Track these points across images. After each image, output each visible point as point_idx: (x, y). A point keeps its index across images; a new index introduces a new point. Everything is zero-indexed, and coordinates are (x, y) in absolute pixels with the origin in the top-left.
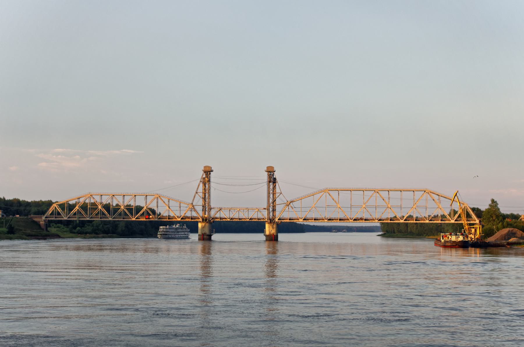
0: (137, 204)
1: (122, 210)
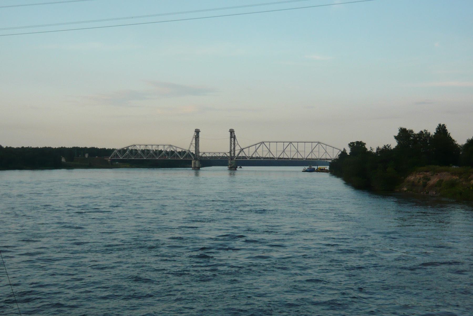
0: (160, 149)
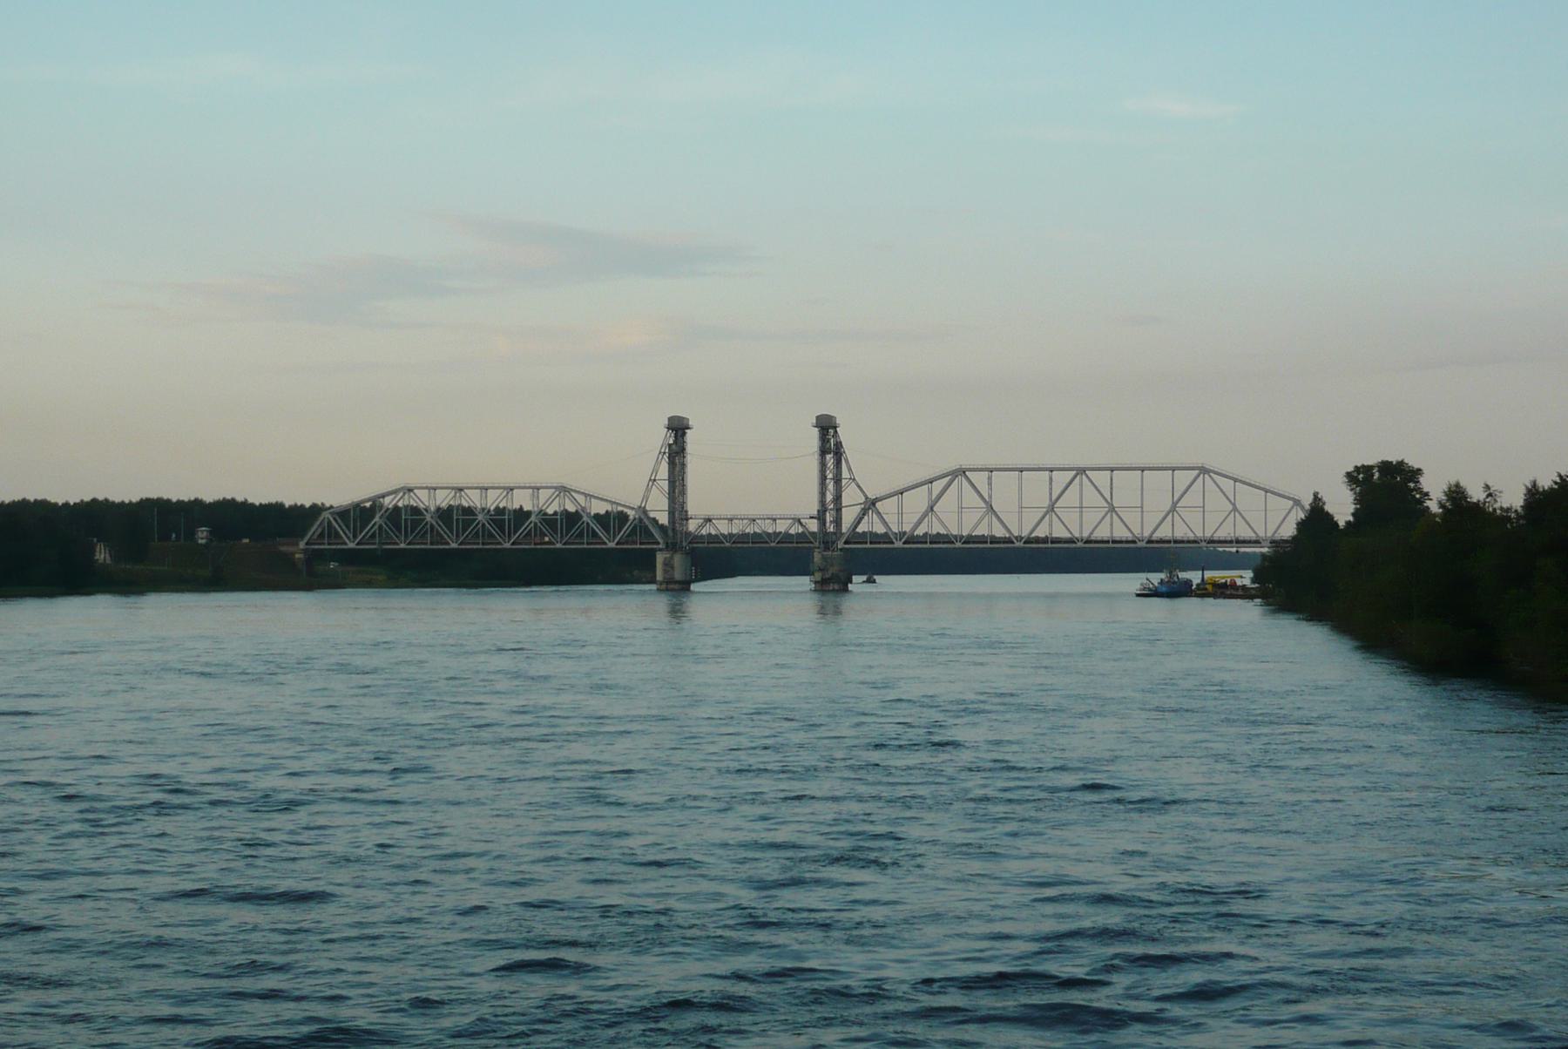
1: (376, 527)
